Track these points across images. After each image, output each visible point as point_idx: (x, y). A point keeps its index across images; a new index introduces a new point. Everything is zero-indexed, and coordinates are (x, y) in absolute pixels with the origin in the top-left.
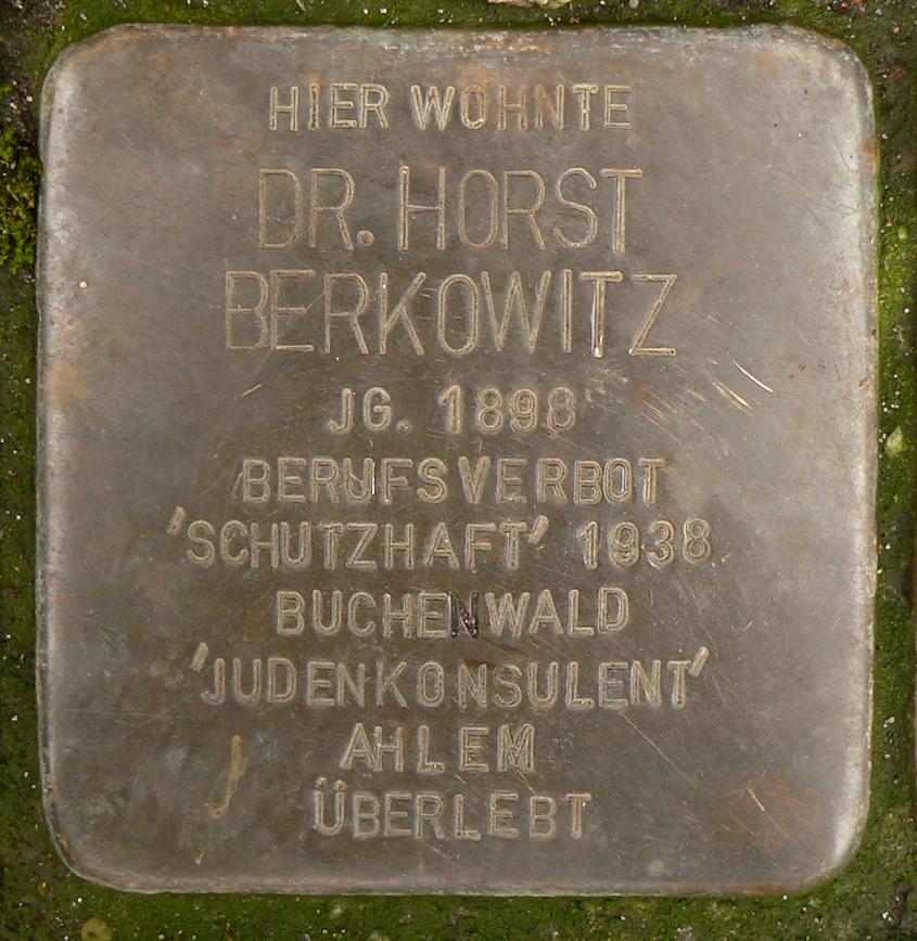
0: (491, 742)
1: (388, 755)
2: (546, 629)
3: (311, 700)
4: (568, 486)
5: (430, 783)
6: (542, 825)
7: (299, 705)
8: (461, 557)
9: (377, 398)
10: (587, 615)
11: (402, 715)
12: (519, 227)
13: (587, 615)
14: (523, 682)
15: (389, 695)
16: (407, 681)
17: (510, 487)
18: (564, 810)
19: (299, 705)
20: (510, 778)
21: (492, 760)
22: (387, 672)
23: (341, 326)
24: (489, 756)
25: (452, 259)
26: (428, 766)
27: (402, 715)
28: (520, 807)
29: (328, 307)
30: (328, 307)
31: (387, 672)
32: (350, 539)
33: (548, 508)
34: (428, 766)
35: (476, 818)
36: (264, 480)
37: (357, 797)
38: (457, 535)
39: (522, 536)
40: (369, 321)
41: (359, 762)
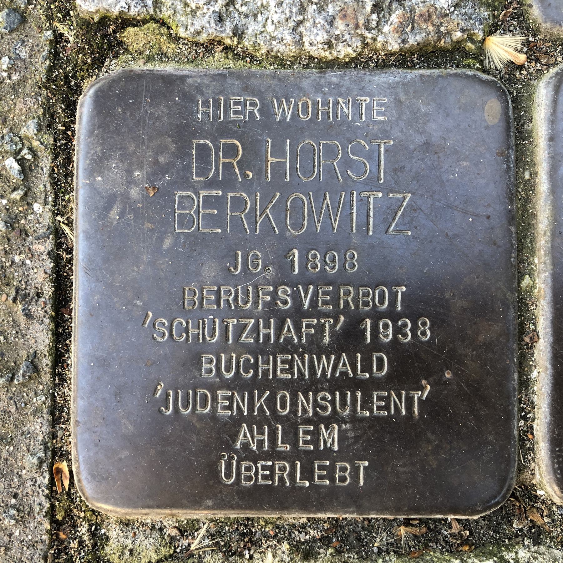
0: (316, 434)
1: (261, 443)
2: (344, 374)
3: (221, 412)
4: (356, 300)
5: (280, 456)
6: (343, 479)
7: (213, 415)
8: (300, 337)
9: (256, 257)
10: (367, 368)
11: (266, 421)
12: (330, 170)
13: (367, 368)
14: (333, 402)
15: (261, 409)
16: (271, 402)
17: (325, 303)
18: (356, 470)
19: (213, 415)
20: (328, 453)
21: (317, 445)
22: (260, 397)
23: (237, 221)
24: (315, 441)
25: (296, 186)
26: (283, 447)
27: (266, 421)
28: (331, 470)
29: (325, 142)
30: (325, 142)
31: (260, 397)
32: (240, 329)
33: (346, 311)
34: (283, 447)
35: (308, 474)
36: (213, 366)
37: (244, 464)
38: (298, 327)
39: (333, 327)
40: (252, 218)
41: (246, 446)
